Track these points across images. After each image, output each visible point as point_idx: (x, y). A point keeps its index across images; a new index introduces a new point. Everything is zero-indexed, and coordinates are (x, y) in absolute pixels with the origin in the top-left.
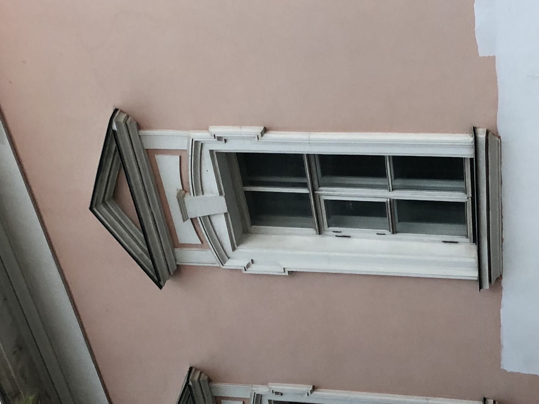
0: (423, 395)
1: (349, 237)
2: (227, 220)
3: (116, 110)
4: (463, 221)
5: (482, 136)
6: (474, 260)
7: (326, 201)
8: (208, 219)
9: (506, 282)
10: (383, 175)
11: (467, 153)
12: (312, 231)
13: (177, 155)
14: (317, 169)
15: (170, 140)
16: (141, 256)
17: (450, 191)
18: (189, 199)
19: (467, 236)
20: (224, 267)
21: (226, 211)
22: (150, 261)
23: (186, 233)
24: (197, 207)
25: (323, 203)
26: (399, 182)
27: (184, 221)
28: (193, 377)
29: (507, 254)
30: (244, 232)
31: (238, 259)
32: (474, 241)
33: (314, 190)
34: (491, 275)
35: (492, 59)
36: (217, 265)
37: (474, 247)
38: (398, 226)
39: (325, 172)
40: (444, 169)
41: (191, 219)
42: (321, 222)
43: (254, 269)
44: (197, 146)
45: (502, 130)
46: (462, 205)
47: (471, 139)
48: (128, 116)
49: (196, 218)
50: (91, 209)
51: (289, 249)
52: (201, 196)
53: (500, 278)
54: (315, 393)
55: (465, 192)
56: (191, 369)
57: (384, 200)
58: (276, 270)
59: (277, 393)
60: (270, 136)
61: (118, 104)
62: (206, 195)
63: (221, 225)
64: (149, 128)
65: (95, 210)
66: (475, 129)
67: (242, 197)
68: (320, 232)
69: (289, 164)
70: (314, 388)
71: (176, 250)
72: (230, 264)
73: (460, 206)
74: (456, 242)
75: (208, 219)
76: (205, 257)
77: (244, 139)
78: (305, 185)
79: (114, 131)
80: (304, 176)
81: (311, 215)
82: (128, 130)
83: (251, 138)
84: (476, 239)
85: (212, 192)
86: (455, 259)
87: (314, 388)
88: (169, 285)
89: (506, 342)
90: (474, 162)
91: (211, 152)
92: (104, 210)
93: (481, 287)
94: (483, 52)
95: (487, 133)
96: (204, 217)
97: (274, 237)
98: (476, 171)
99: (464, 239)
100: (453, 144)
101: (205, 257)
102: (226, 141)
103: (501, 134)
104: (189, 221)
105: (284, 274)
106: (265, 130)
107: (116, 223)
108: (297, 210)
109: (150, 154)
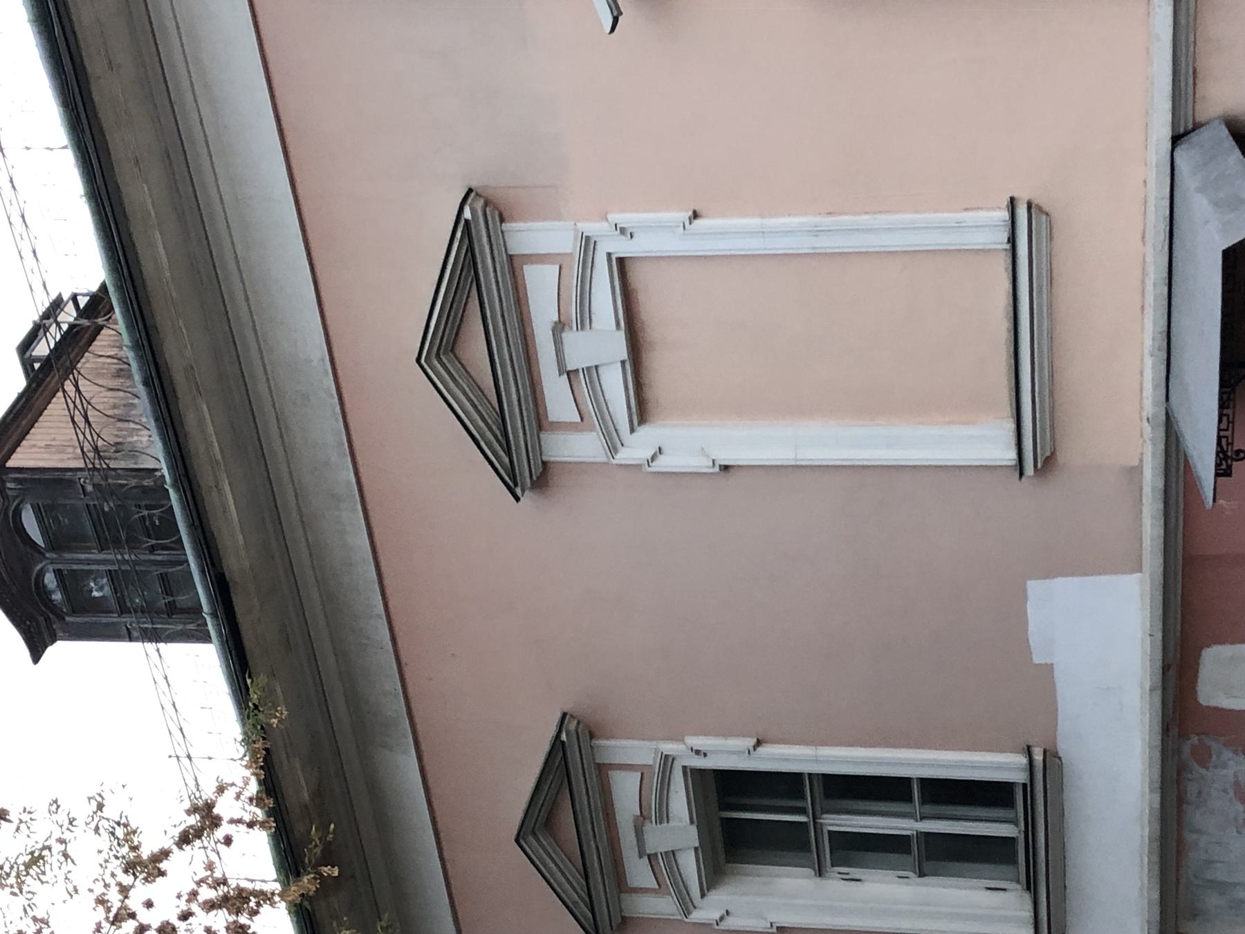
3: (564, 715)
4: (1014, 862)
5: (1038, 757)
6: (1028, 914)
8: (593, 372)
10: (908, 799)
11: (1019, 777)
13: (553, 263)
15: (632, 752)
16: (575, 903)
18: (571, 338)
19: (1018, 882)
20: (614, 462)
22: (590, 915)
23: (639, 873)
24: (658, 839)
26: (928, 809)
27: (641, 857)
29: (1071, 819)
30: (715, 872)
31: (706, 912)
32: (1028, 888)
33: (814, 818)
37: (1027, 899)
38: (928, 866)
39: (828, 794)
41: (649, 856)
42: (821, 847)
43: (731, 923)
44: (588, 244)
45: (1063, 748)
46: (1012, 840)
48: (579, 723)
50: (517, 841)
52: (665, 824)
54: (759, 749)
55: (1016, 823)
57: (908, 833)
60: (764, 750)
61: (568, 707)
63: (689, 865)
64: (512, 220)
65: (523, 843)
66: (1029, 747)
68: (820, 873)
69: (785, 786)
71: (623, 896)
72: (697, 916)
73: (1009, 842)
75: (593, 372)
77: (729, 753)
78: (802, 811)
79: (563, 742)
80: (803, 797)
81: (809, 850)
83: (739, 753)
84: (1031, 885)
85: (681, 820)
86: (1002, 912)
90: (1028, 788)
91: (684, 768)
93: (1021, 474)
94: (1038, 659)
96: (588, 368)
98: (1034, 866)
99: (1013, 885)
100: (1003, 765)
101: (664, 906)
102: (705, 755)
103: (1061, 754)
104: (646, 858)
105: (711, 470)
106: (759, 743)
107: (548, 860)
108: (789, 845)
109: (603, 770)
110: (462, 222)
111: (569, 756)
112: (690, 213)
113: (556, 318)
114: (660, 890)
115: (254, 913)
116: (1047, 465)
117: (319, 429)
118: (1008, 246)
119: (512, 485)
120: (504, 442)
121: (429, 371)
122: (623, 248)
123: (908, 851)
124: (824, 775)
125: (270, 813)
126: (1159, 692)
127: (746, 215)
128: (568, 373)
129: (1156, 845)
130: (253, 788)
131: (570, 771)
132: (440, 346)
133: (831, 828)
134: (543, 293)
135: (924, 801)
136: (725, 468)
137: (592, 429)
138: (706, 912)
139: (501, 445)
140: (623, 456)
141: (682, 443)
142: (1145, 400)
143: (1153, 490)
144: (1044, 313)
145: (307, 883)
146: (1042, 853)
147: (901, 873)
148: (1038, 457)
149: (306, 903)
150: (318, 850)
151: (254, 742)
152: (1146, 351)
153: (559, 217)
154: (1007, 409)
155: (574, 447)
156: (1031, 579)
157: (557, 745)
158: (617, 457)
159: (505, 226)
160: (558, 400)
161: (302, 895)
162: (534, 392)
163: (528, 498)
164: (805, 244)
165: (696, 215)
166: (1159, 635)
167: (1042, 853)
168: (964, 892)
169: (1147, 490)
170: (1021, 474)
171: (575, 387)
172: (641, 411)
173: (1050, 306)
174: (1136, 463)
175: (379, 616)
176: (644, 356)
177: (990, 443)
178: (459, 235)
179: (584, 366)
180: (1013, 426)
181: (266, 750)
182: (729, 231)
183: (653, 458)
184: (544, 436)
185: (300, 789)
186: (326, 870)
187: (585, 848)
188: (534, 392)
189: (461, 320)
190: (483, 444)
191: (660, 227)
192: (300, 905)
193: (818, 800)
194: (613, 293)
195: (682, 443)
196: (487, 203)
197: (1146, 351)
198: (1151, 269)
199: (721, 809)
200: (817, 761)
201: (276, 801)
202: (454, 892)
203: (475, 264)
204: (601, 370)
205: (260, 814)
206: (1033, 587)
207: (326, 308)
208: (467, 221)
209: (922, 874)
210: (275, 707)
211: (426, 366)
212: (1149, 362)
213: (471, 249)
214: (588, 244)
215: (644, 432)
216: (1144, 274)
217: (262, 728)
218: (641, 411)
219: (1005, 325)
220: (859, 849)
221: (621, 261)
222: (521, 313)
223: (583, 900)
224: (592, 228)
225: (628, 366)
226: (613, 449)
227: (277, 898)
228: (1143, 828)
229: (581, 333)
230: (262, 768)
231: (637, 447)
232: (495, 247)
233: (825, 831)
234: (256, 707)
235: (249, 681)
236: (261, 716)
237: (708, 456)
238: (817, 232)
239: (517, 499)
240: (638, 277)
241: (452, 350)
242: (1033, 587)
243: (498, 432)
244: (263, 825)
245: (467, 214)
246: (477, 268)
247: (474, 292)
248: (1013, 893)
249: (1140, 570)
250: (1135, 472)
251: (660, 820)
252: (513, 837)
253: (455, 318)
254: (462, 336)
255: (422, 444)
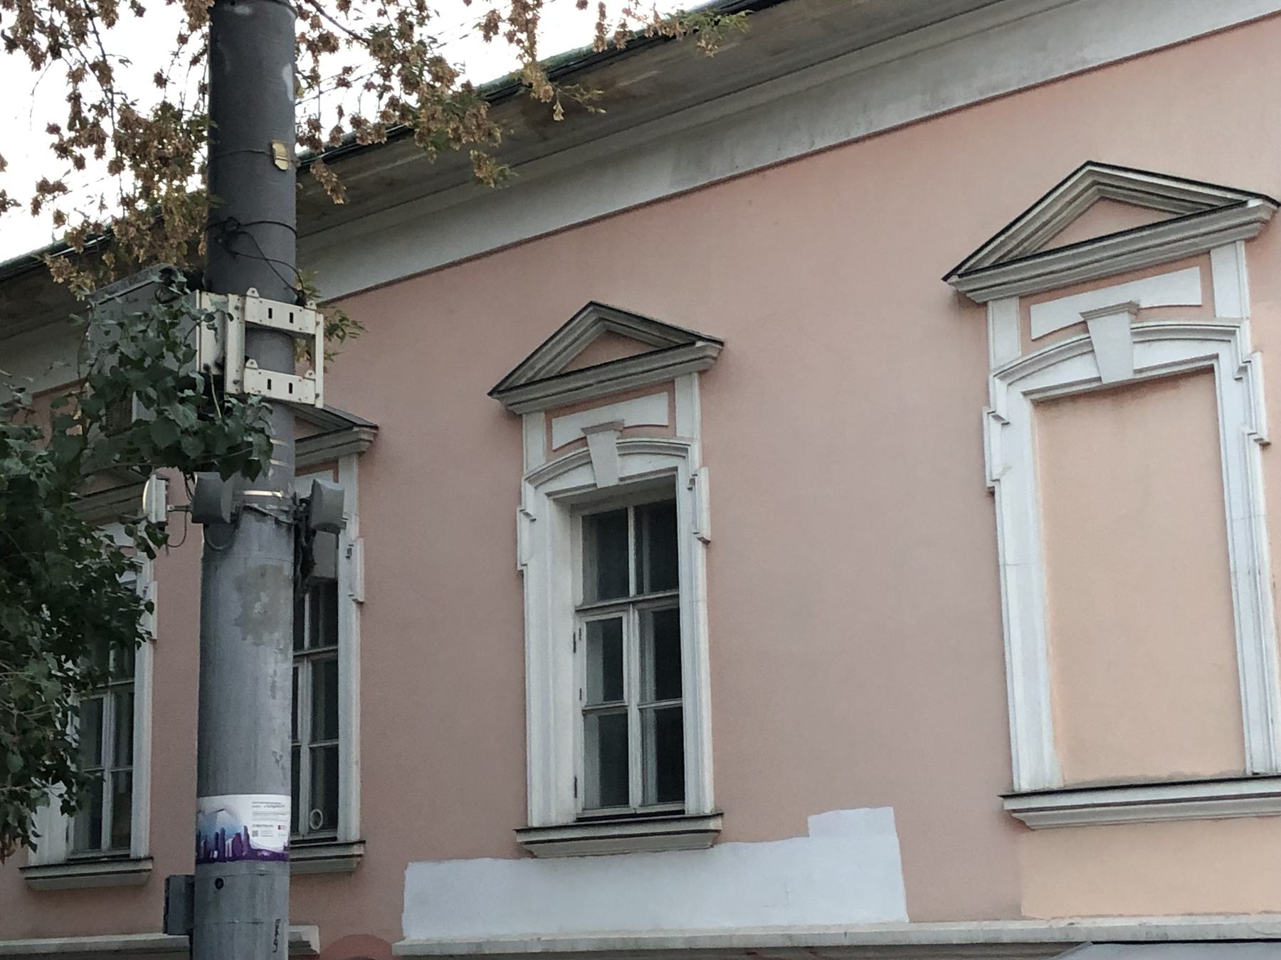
0: (362, 756)
1: (575, 650)
2: (589, 486)
3: (721, 343)
4: (604, 804)
5: (712, 824)
6: (555, 820)
7: (621, 618)
8: (1087, 349)
9: (528, 862)
11: (691, 806)
12: (579, 599)
14: (665, 605)
15: (688, 412)
16: (532, 367)
17: (642, 785)
18: (1123, 323)
19: (584, 809)
20: (991, 377)
21: (1105, 381)
22: (522, 382)
23: (567, 429)
24: (603, 446)
25: (620, 614)
26: (651, 716)
28: (365, 432)
29: (649, 860)
31: (534, 500)
32: (579, 820)
33: (634, 603)
34: (534, 843)
35: (803, 832)
36: (993, 365)
37: (569, 820)
38: (594, 718)
39: (657, 615)
40: (671, 776)
43: (992, 427)
44: (1227, 334)
45: (723, 850)
46: (625, 801)
47: (708, 812)
48: (715, 359)
49: (587, 445)
50: (591, 303)
51: (554, 572)
52: (617, 453)
53: (532, 855)
54: (354, 605)
55: (643, 805)
56: (376, 428)
58: (995, 466)
59: (349, 551)
60: (700, 549)
62: (618, 459)
63: (579, 479)
64: (1250, 256)
65: (590, 309)
66: (721, 815)
67: (617, 506)
68: (579, 611)
69: (665, 572)
70: (360, 604)
72: (528, 489)
73: (624, 799)
74: (576, 796)
75: (1087, 349)
76: (535, 455)
77: (694, 515)
78: (640, 590)
79: (694, 343)
80: (654, 589)
82: (1226, 229)
83: (694, 522)
84: (582, 822)
87: (360, 604)
88: (495, 403)
89: (445, 867)
90: (680, 816)
91: (676, 469)
92: (590, 321)
94: (812, 820)
95: (360, 856)
96: (1091, 342)
97: (568, 548)
100: (702, 788)
101: (535, 455)
105: (988, 478)
106: (706, 542)
107: (570, 339)
108: (606, 579)
110: (1244, 199)
111: (682, 350)
112: (1267, 440)
113: (1143, 305)
114: (551, 451)
115: (510, 37)
116: (1017, 823)
117: (1009, 66)
118: (1249, 774)
119: (961, 271)
120: (1005, 260)
121: (1080, 174)
122: (1225, 370)
123: (607, 697)
124: (678, 610)
125: (611, 45)
126: (789, 944)
127: (1268, 500)
128: (1084, 322)
129: (632, 946)
130: (635, 26)
131: (661, 351)
132: (1106, 185)
133: (624, 620)
134: (1174, 289)
135: (658, 712)
136: (521, 574)
137: (1025, 351)
138: (534, 500)
139: (1001, 258)
140: (998, 388)
141: (1015, 447)
142: (1091, 920)
143: (1001, 931)
144: (1117, 820)
145: (545, 90)
146: (616, 831)
147: (585, 691)
148: (1023, 813)
149: (522, 90)
150: (578, 98)
151: (681, 23)
152: (1144, 920)
153: (1254, 301)
154: (1071, 782)
155: (1004, 335)
156: (897, 814)
157: (691, 339)
158: (997, 381)
159: (1241, 247)
160: (1054, 314)
161: (531, 85)
162: (1066, 287)
163: (947, 289)
164: (1240, 560)
165: (1265, 445)
166: (846, 942)
167: (616, 831)
168: (570, 753)
169: (997, 925)
170: (1004, 797)
171: (1064, 332)
172: (1046, 402)
173: (1191, 819)
174: (1024, 913)
175: (849, 134)
176: (1106, 401)
177: (1037, 762)
178: (1229, 195)
179: (1093, 339)
180: (1055, 787)
181: (674, 37)
182: (1248, 481)
183: (998, 418)
184: (1015, 302)
185: (630, 77)
186: (558, 107)
187: (588, 373)
188: (1050, 290)
189: (1135, 205)
190: (1002, 238)
191: (1249, 408)
192: (521, 84)
193: (652, 605)
194: (1192, 361)
195: (1015, 447)
196: (1265, 222)
197: (1144, 920)
198: (1233, 921)
199: (636, 508)
200: (692, 602)
201: (622, 52)
202: (631, 214)
203: (1199, 215)
204: (1088, 358)
205: (610, 35)
206: (888, 813)
207: (1241, 32)
208: (1246, 202)
209: (585, 713)
210: (718, 42)
211: (1084, 171)
212: (1133, 922)
213: (1215, 210)
214: (1227, 334)
215: (1026, 406)
216: (1227, 915)
217: (696, 31)
218: (1046, 402)
219: (1163, 774)
220: (604, 647)
221: (1210, 370)
222: (1129, 272)
223: (536, 374)
224: (1245, 337)
225: (1094, 385)
226: (1004, 375)
227: (527, 59)
228: (648, 932)
229: (1128, 332)
230: (656, 33)
231: (1008, 400)
232: (1224, 233)
233: (620, 614)
234: (716, 23)
235: (743, 13)
236: (708, 28)
237: (1003, 473)
238: (1254, 572)
239: (945, 279)
240: (1192, 392)
241: (1103, 198)
242: (888, 813)
243: (1015, 253)
244: (600, 39)
245: (1253, 203)
246: (1190, 216)
247: (1175, 216)
248: (572, 805)
249: (912, 921)
250: (1016, 913)
251: (621, 447)
252: (594, 300)
253: (1137, 198)
254: (1118, 207)
255: (999, 174)
